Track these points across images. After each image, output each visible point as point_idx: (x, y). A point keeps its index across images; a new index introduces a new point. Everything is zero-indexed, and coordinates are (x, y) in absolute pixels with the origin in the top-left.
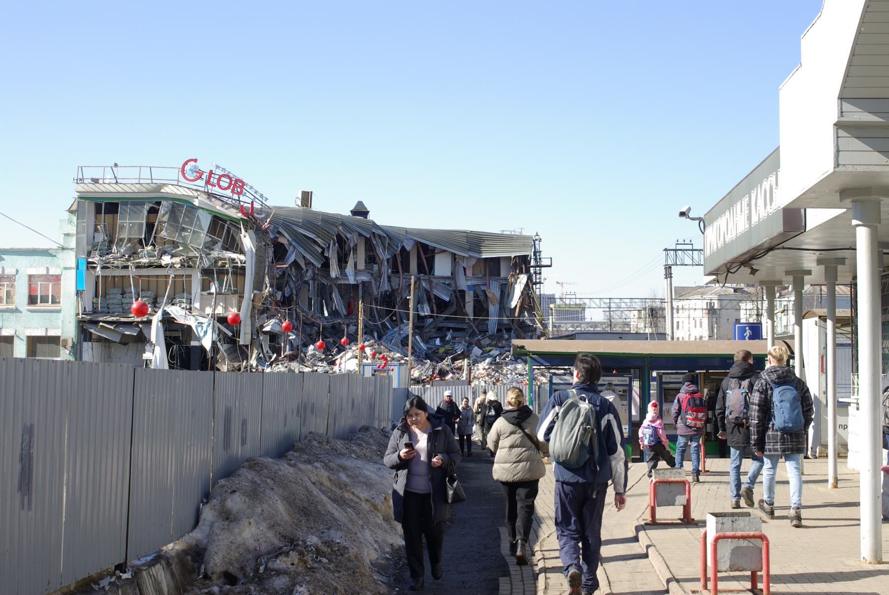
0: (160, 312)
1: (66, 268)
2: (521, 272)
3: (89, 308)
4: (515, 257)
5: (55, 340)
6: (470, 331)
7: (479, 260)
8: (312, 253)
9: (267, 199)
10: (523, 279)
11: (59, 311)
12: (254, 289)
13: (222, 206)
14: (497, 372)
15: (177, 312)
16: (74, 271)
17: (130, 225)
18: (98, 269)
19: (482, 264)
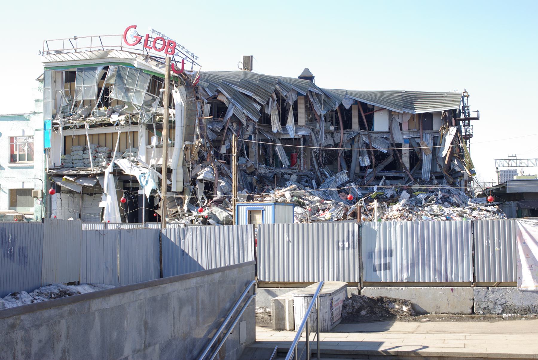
0: (111, 164)
1: (37, 130)
2: (451, 125)
3: (59, 164)
4: (445, 111)
5: (27, 192)
6: (407, 179)
7: (414, 116)
8: (252, 110)
9: (197, 58)
10: (453, 130)
11: (32, 167)
12: (186, 140)
13: (157, 65)
14: (410, 212)
15: (125, 165)
16: (42, 132)
17: (87, 88)
18: (60, 129)
19: (416, 120)
